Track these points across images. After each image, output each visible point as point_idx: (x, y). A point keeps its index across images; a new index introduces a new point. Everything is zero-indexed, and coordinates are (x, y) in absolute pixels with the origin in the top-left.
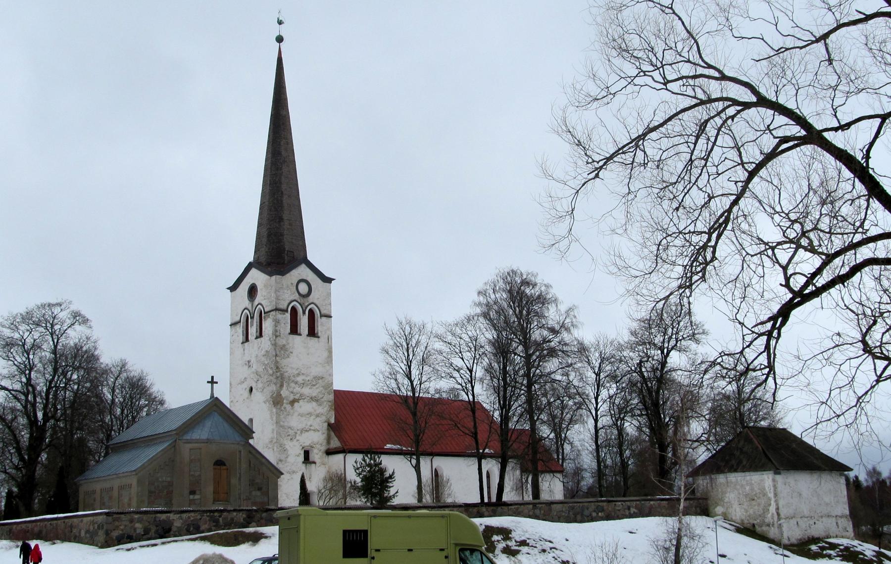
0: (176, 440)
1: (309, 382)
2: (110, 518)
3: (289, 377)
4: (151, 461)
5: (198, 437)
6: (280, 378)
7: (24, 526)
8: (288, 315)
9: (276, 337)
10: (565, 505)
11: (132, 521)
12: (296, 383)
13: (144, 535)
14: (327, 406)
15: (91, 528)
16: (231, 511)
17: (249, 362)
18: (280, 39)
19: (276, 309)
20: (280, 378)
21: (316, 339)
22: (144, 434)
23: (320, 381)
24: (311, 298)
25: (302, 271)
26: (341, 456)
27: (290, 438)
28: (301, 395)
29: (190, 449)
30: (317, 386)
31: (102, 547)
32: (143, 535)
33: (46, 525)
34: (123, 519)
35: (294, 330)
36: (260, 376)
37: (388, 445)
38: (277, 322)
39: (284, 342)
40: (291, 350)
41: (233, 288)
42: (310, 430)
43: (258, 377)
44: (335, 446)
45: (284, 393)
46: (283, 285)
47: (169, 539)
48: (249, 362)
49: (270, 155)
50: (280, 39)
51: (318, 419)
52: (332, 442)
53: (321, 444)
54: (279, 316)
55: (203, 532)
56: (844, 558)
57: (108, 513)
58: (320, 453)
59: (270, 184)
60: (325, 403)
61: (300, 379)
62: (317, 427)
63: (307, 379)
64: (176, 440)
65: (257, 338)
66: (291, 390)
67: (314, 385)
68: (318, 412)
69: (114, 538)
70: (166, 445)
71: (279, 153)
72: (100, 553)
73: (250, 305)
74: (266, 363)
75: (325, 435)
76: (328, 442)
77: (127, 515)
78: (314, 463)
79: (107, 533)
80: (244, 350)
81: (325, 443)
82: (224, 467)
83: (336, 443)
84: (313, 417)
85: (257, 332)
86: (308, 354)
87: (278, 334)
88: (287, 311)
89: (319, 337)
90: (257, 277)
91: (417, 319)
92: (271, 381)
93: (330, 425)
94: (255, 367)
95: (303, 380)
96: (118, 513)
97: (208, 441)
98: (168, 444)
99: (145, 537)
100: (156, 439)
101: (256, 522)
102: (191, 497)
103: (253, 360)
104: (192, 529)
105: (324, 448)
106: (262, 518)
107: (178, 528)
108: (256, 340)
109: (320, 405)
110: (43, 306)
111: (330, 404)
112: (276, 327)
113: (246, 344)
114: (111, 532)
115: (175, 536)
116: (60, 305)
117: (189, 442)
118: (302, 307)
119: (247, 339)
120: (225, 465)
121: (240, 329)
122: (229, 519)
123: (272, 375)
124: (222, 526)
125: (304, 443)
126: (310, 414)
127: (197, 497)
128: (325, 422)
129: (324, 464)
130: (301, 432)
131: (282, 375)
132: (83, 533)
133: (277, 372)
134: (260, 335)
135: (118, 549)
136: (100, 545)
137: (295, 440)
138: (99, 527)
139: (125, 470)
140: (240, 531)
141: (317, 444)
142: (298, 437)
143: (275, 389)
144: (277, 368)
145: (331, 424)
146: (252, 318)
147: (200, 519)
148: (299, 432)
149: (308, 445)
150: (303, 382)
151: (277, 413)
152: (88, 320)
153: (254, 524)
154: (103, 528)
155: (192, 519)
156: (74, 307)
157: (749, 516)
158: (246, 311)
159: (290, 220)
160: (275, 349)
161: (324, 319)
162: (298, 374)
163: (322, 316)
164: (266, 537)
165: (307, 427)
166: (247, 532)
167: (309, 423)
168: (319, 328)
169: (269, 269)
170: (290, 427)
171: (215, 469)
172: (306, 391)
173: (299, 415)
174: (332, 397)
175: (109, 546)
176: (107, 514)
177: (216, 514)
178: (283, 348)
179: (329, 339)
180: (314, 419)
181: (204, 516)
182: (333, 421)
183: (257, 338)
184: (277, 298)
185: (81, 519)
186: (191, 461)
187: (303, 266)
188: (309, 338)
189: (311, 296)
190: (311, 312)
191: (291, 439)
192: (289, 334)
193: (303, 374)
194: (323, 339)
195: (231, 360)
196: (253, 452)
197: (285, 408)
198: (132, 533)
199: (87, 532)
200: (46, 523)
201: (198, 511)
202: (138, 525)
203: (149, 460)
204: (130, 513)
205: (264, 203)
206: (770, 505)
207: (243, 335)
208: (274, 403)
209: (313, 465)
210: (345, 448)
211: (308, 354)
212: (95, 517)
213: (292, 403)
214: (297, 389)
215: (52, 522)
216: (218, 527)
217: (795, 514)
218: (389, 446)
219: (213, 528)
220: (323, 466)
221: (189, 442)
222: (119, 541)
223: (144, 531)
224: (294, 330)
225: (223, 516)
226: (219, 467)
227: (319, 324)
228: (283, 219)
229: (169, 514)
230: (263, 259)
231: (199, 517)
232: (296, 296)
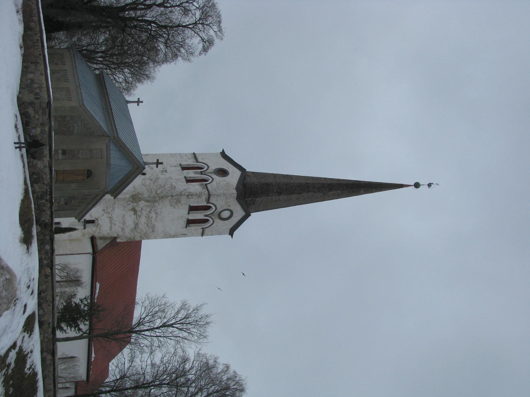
0: (109, 137)
1: (150, 221)
2: (45, 106)
3: (155, 207)
4: (92, 117)
5: (111, 156)
6: (154, 199)
7: (35, 11)
8: (205, 204)
9: (188, 196)
11: (43, 125)
12: (150, 212)
13: (30, 135)
14: (130, 236)
15: (36, 86)
16: (52, 209)
18: (417, 185)
19: (209, 195)
20: (154, 199)
21: (185, 226)
22: (112, 104)
23: (151, 230)
24: (217, 221)
25: (239, 213)
26: (90, 250)
27: (105, 209)
28: (140, 216)
29: (101, 149)
30: (147, 227)
31: (19, 99)
32: (30, 135)
33: (37, 34)
34: (44, 118)
35: (192, 209)
36: (155, 182)
37: (99, 284)
38: (199, 196)
39: (183, 202)
41: (223, 154)
42: (112, 224)
43: (154, 180)
44: (98, 244)
45: (142, 204)
46: (229, 199)
47: (26, 160)
48: (166, 171)
49: (329, 182)
50: (417, 185)
51: (120, 230)
52: (101, 241)
53: (99, 233)
54: (204, 197)
55: (32, 186)
57: (50, 104)
58: (92, 232)
59: (307, 183)
60: (133, 234)
61: (153, 215)
62: (113, 229)
63: (153, 220)
64: (109, 137)
65: (185, 177)
66: (144, 208)
67: (147, 225)
68: (126, 229)
69: (27, 110)
70: (105, 128)
71: (331, 190)
72: (13, 101)
73: (211, 171)
74: (166, 187)
75: (107, 235)
76: (101, 238)
77: (48, 120)
78: (85, 228)
79: (32, 104)
80: (175, 166)
81: (100, 235)
82: (86, 178)
83: (101, 245)
84: (122, 226)
85: (190, 177)
86: (173, 220)
87: (190, 197)
88: (208, 203)
89: (186, 227)
90: (234, 176)
91: (210, 331)
92: (151, 192)
93: (115, 238)
94: (162, 176)
95: (152, 217)
96: (50, 113)
97: (108, 164)
98: (106, 130)
99: (28, 137)
100: (109, 116)
101: (41, 231)
102: (60, 152)
103: (167, 175)
104: (35, 177)
105: (96, 235)
106: (44, 236)
107: (36, 165)
110: (219, 16)
111: (132, 238)
112: (196, 195)
113: (180, 168)
114: (33, 107)
115: (28, 163)
116: (220, 30)
117: (108, 148)
118: (211, 214)
119: (184, 168)
120: (88, 177)
121: (191, 162)
122: (44, 208)
123: (156, 193)
124: (37, 202)
125: (101, 220)
126: (124, 223)
127: (60, 156)
128: (118, 235)
129: (83, 235)
130: (110, 217)
131: (156, 201)
132: (30, 76)
133: (159, 197)
135: (16, 116)
136: (20, 96)
137: (103, 213)
138: (37, 94)
139: (84, 94)
140: (33, 223)
141: (100, 230)
142: (105, 215)
143: (145, 196)
144: (162, 197)
145: (116, 239)
146: (201, 173)
147: (44, 184)
148: (110, 215)
149: (100, 223)
150: (150, 217)
151: (125, 198)
152: (207, 52)
153: (40, 229)
154: (36, 99)
155: (44, 176)
156: (217, 41)
158: (206, 167)
159: (279, 200)
160: (177, 195)
161: (201, 231)
162: (156, 213)
163: (203, 229)
164: (28, 249)
165: (114, 221)
166: (33, 229)
168: (193, 228)
169: (241, 187)
171: (84, 170)
172: (143, 220)
173: (124, 215)
174: (138, 239)
175: (19, 105)
176: (49, 103)
177: (48, 197)
178: (178, 201)
179: (184, 235)
180: (120, 227)
181: (47, 186)
182: (118, 240)
183: (185, 177)
184: (218, 195)
185: (43, 72)
187: (243, 214)
188: (186, 220)
189: (219, 220)
190: (206, 221)
191: (104, 210)
192: (190, 205)
193: (157, 217)
194: (185, 231)
195: (166, 154)
196: (98, 198)
197: (129, 204)
200: (39, 35)
201: (52, 181)
202: (38, 130)
203: (92, 116)
204: (50, 123)
205: (292, 179)
207: (187, 165)
208: (133, 195)
209: (83, 227)
210: (97, 254)
211: (173, 220)
212: (46, 89)
213: (134, 210)
214: (145, 213)
215: (40, 41)
216: (36, 199)
218: (98, 285)
219: (36, 195)
220: (82, 234)
221: (108, 148)
222: (24, 114)
223: (33, 135)
224: (192, 209)
225: (47, 202)
226: (86, 173)
227: (197, 227)
228: (280, 195)
229: (48, 156)
230: (248, 180)
231: (46, 182)
232: (219, 209)
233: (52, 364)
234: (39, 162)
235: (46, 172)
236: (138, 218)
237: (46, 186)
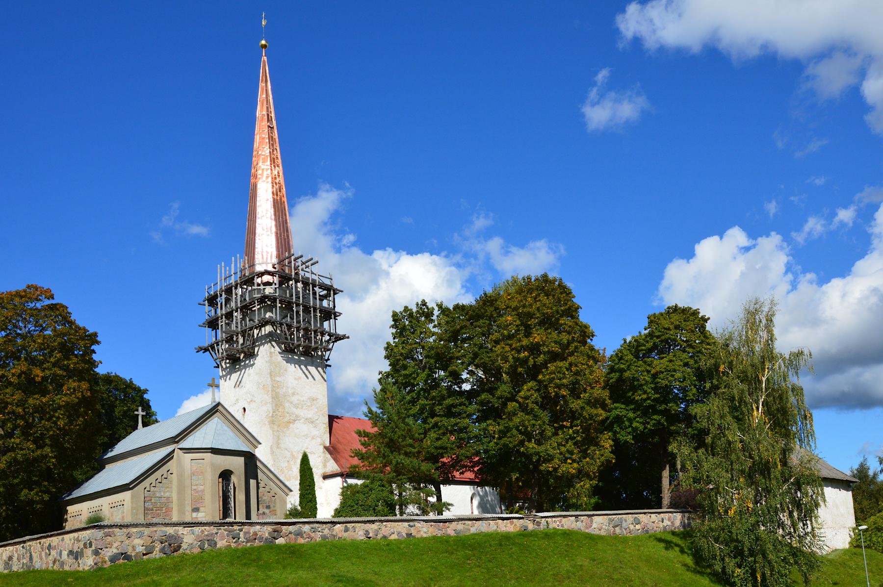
10: (606, 517)
11: (129, 536)
14: (322, 428)
52: (328, 464)
61: (295, 399)
76: (325, 466)
104: (206, 546)
109: (315, 427)
128: (321, 445)
138: (85, 544)
147: (217, 533)
154: (91, 546)
155: (206, 533)
162: (294, 394)
177: (236, 527)
182: (328, 444)
186: (193, 474)
199: (71, 552)
202: (137, 542)
233: (463, 522)
234: (185, 540)
235: (200, 531)
236: (298, 419)
237: (220, 531)
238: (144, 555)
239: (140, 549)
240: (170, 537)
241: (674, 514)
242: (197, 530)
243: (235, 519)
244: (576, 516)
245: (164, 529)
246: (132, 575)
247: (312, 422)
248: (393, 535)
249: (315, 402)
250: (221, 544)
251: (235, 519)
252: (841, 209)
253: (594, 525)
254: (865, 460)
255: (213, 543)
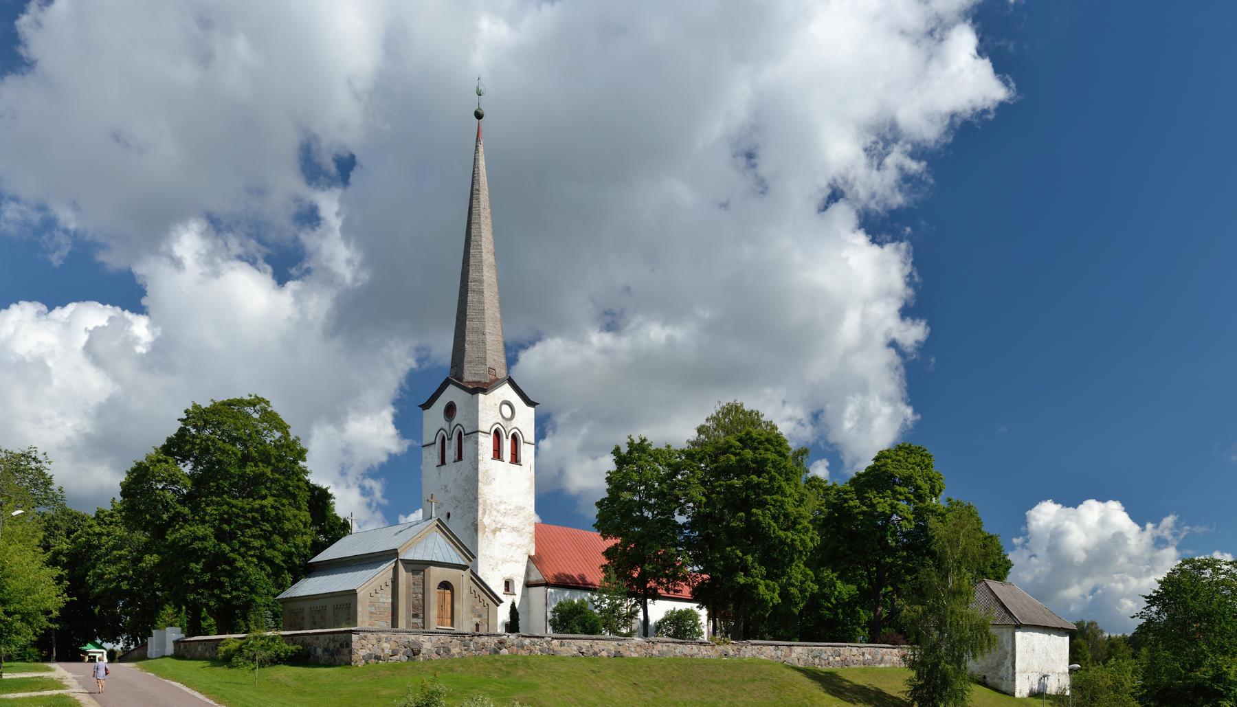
10: (805, 648)
17: (446, 487)
24: (514, 423)
36: (459, 502)
40: (493, 476)
43: (457, 503)
46: (486, 404)
56: (868, 701)
66: (493, 518)
67: (516, 515)
68: (518, 543)
84: (514, 548)
85: (455, 455)
108: (454, 464)
109: (521, 536)
113: (442, 467)
125: (505, 574)
126: (511, 545)
134: (460, 458)
142: (499, 568)
146: (450, 439)
147: (451, 642)
148: (500, 562)
157: (981, 668)
162: (501, 502)
163: (524, 442)
167: (510, 554)
170: (491, 557)
173: (501, 544)
182: (533, 553)
197: (487, 537)
198: (379, 653)
202: (386, 645)
206: (1006, 658)
213: (494, 532)
214: (500, 518)
217: (1027, 668)
224: (497, 454)
232: (500, 420)
233: (667, 644)
238: (391, 656)
239: (388, 651)
240: (414, 643)
241: (877, 649)
242: (434, 638)
243: (452, 624)
244: (777, 646)
245: (407, 635)
246: (362, 675)
247: (518, 531)
248: (603, 652)
249: (522, 511)
250: (455, 651)
251: (452, 624)
252: (965, 111)
253: (794, 655)
254: (847, 199)
255: (448, 651)
